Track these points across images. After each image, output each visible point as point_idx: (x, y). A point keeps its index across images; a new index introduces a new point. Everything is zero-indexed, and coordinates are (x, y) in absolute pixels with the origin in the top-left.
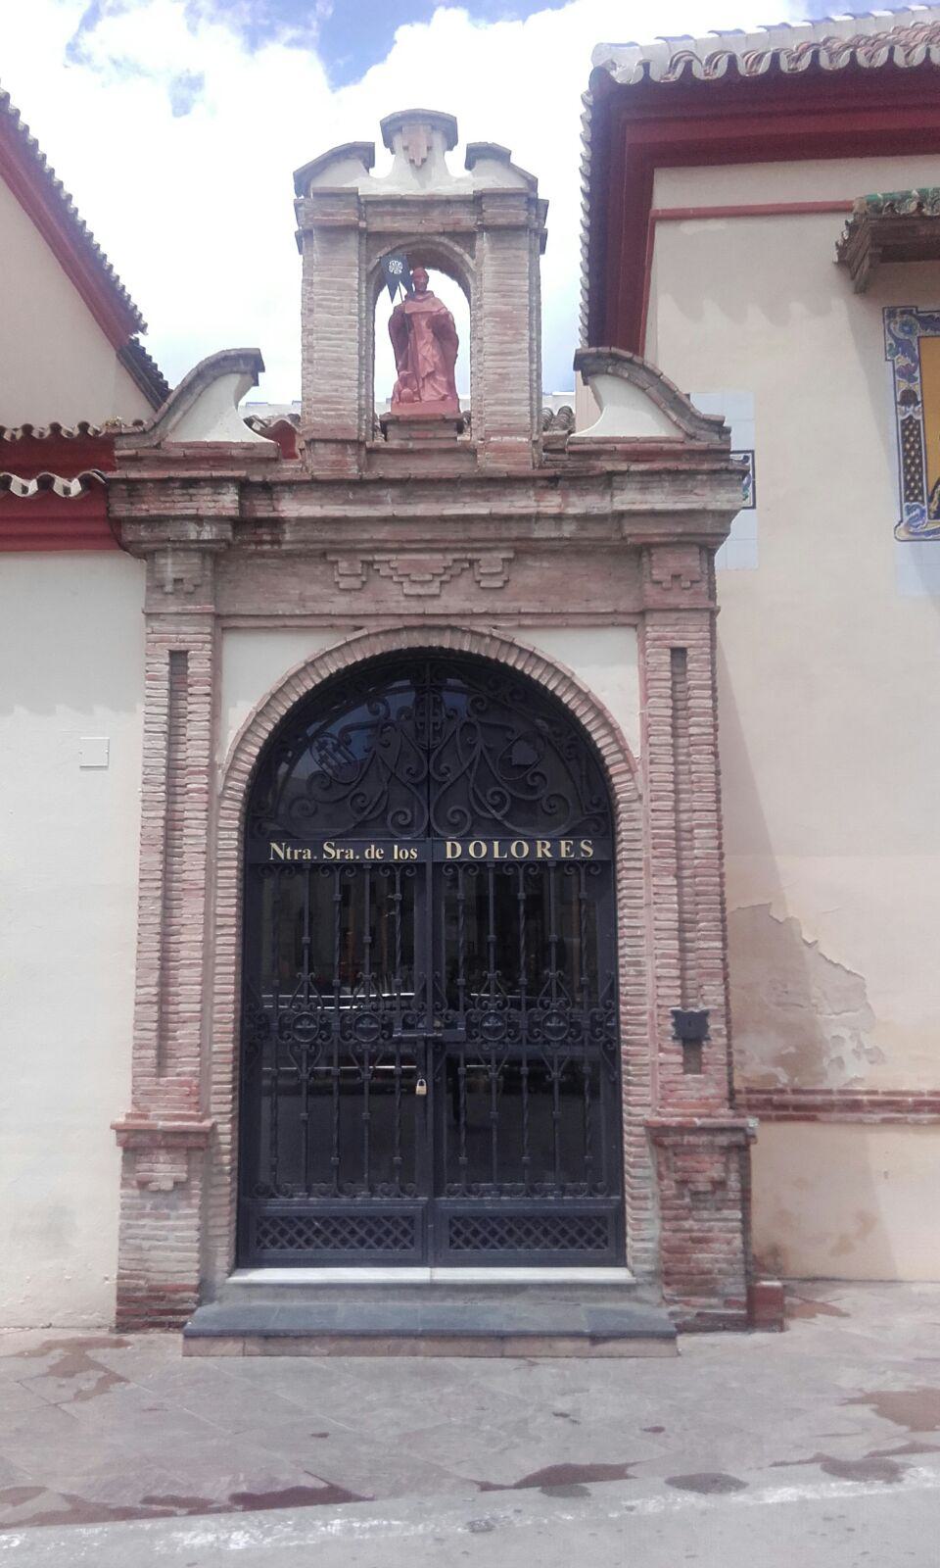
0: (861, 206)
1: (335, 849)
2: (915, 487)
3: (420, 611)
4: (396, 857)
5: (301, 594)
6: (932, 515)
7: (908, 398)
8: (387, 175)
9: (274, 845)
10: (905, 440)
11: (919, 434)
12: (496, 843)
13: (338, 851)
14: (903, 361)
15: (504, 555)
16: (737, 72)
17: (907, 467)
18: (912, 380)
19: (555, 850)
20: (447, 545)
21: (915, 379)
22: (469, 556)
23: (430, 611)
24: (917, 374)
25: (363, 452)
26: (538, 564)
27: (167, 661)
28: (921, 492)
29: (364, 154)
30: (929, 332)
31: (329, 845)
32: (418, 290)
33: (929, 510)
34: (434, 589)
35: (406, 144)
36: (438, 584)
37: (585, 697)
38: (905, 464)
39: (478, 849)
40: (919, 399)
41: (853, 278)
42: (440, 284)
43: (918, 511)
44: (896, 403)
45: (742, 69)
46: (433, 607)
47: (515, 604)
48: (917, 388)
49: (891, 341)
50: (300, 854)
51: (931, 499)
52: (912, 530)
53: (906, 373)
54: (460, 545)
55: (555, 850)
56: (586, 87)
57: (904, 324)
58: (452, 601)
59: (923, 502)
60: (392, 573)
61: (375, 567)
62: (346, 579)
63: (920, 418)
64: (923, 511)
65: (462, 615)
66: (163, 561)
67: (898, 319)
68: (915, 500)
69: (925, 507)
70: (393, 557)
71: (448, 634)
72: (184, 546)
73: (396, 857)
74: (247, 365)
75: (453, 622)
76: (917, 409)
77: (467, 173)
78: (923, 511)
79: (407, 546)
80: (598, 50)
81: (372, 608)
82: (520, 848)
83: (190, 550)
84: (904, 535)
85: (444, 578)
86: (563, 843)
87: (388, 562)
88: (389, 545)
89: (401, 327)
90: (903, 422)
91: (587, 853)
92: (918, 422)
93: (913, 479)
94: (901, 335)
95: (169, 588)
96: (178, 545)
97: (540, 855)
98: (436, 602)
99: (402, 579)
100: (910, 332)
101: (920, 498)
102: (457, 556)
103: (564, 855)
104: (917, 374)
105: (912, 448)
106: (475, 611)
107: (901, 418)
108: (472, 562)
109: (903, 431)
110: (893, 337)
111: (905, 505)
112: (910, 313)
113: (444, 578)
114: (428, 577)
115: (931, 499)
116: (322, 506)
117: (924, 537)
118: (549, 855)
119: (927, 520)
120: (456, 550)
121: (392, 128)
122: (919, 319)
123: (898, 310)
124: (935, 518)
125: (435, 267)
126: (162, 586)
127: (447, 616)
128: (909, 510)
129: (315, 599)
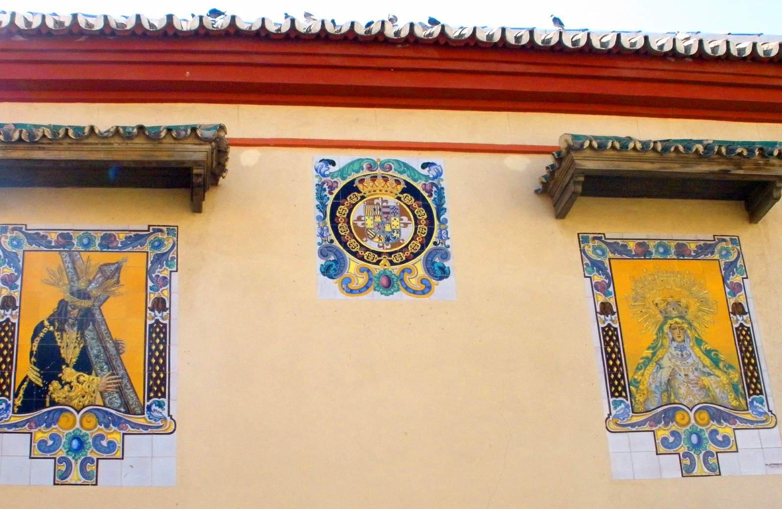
2: (156, 379)
6: (16, 410)
7: (606, 309)
10: (607, 344)
11: (617, 340)
14: (598, 278)
18: (607, 294)
21: (16, 287)
24: (18, 283)
30: (34, 247)
33: (14, 405)
38: (164, 359)
40: (18, 305)
44: (596, 313)
49: (586, 261)
51: (16, 395)
57: (595, 249)
59: (9, 397)
64: (8, 406)
67: (9, 235)
68: (620, 395)
69: (11, 402)
76: (14, 312)
78: (8, 406)
92: (14, 324)
93: (616, 378)
94: (594, 257)
101: (7, 393)
104: (18, 283)
107: (601, 325)
111: (611, 400)
112: (20, 230)
115: (16, 395)
117: (6, 429)
119: (11, 414)
122: (26, 235)
123: (10, 227)
124: (19, 412)
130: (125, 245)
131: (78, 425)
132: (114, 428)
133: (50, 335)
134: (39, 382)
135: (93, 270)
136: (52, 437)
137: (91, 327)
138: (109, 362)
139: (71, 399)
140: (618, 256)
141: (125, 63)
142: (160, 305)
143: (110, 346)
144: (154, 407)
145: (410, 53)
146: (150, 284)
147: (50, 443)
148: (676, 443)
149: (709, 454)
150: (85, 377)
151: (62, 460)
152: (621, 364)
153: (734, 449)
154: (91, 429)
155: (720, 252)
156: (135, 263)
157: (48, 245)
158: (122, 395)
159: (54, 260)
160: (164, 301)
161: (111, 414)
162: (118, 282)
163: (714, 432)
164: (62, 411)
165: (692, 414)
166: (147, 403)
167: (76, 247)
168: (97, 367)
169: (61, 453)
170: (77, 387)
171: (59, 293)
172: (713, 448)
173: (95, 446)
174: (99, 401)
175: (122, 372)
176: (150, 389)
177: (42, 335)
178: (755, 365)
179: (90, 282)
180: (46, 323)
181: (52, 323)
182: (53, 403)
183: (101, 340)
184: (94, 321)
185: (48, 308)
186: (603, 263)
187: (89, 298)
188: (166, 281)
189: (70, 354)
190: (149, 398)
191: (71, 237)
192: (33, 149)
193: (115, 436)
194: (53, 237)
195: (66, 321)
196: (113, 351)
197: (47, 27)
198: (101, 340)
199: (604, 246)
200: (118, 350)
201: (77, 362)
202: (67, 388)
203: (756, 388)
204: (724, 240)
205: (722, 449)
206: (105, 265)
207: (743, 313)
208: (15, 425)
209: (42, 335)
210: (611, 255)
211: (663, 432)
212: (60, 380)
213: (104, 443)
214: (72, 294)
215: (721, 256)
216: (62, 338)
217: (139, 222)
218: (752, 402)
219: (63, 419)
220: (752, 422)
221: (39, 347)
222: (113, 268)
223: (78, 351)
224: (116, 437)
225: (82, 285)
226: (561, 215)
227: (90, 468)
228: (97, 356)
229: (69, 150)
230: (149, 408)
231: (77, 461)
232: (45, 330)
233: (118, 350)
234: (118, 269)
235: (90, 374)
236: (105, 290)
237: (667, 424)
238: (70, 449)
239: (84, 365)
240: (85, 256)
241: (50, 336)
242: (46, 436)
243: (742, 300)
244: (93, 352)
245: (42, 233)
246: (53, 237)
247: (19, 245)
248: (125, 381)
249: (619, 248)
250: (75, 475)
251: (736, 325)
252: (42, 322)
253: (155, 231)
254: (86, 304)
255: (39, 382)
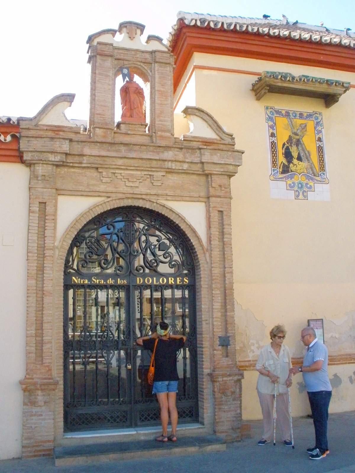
0: (265, 74)
1: (96, 280)
3: (132, 192)
4: (119, 283)
5: (88, 183)
7: (273, 135)
8: (119, 39)
9: (74, 278)
10: (272, 148)
12: (155, 278)
13: (98, 280)
14: (271, 123)
15: (163, 174)
16: (210, 26)
17: (273, 157)
18: (273, 129)
19: (175, 281)
20: (143, 169)
22: (150, 173)
23: (135, 192)
25: (113, 133)
26: (173, 178)
27: (38, 206)
28: (277, 165)
29: (113, 32)
30: (278, 115)
31: (94, 278)
32: (131, 79)
34: (137, 184)
35: (128, 32)
36: (138, 183)
37: (190, 226)
39: (148, 281)
41: (256, 95)
42: (137, 79)
43: (276, 171)
45: (225, 26)
46: (136, 191)
47: (165, 192)
48: (275, 132)
50: (83, 281)
51: (280, 168)
52: (275, 177)
53: (271, 127)
54: (147, 169)
55: (175, 281)
56: (175, 23)
57: (271, 112)
58: (143, 189)
60: (122, 177)
61: (116, 175)
62: (105, 179)
63: (276, 142)
65: (147, 195)
66: (38, 168)
70: (122, 172)
71: (141, 201)
72: (47, 162)
73: (119, 283)
74: (69, 98)
75: (144, 197)
77: (146, 44)
79: (128, 168)
80: (180, 13)
81: (114, 190)
82: (163, 281)
83: (48, 164)
84: (272, 178)
85: (140, 181)
86: (178, 279)
87: (121, 173)
88: (122, 167)
89: (125, 91)
90: (271, 142)
91: (186, 282)
94: (270, 115)
95: (39, 178)
96: (44, 162)
97: (170, 283)
98: (137, 189)
99: (125, 180)
100: (273, 114)
102: (146, 173)
103: (178, 283)
105: (274, 151)
106: (151, 193)
107: (271, 141)
108: (150, 175)
109: (271, 145)
110: (268, 115)
111: (272, 169)
113: (140, 181)
114: (135, 180)
115: (280, 168)
116: (99, 151)
118: (173, 283)
120: (146, 170)
121: (123, 26)
122: (275, 111)
125: (137, 74)
126: (37, 177)
127: (141, 194)
128: (274, 170)
129: (93, 185)
130: (307, 117)
131: (300, 179)
132: (311, 181)
133: (287, 147)
134: (286, 164)
135: (298, 125)
136: (293, 183)
137: (300, 146)
138: (307, 158)
139: (297, 170)
140: (279, 116)
141: (196, 37)
142: (320, 140)
143: (307, 152)
144: (322, 175)
145: (233, 35)
146: (316, 132)
147: (292, 185)
148: (293, 187)
149: (304, 191)
150: (300, 163)
151: (297, 191)
152: (277, 156)
153: (313, 190)
154: (304, 181)
155: (315, 118)
156: (310, 124)
157: (282, 115)
158: (312, 170)
159: (285, 120)
160: (274, 134)
161: (309, 176)
162: (306, 131)
163: (307, 184)
164: (295, 174)
165: (300, 176)
166: (320, 173)
167: (292, 117)
168: (303, 160)
169: (296, 188)
170: (298, 166)
171: (289, 133)
172: (306, 190)
173: (306, 187)
174: (306, 171)
175: (311, 162)
176: (320, 169)
177: (285, 147)
178: (323, 160)
179: (298, 130)
180: (286, 143)
181: (288, 143)
182: (292, 171)
183: (303, 150)
184: (301, 144)
185: (285, 139)
186: (273, 118)
187: (298, 135)
188: (320, 132)
189: (295, 154)
190: (320, 171)
191: (289, 113)
192: (285, 83)
193: (311, 183)
194: (284, 112)
195: (292, 143)
196: (308, 154)
197: (197, 25)
198: (303, 150)
199: (274, 111)
200: (309, 154)
201: (298, 157)
202: (295, 166)
203: (323, 169)
204: (317, 113)
205: (309, 190)
206: (301, 124)
207: (321, 141)
208: (281, 178)
209: (285, 147)
210: (276, 115)
211: (289, 182)
212: (293, 163)
213: (308, 186)
214: (293, 133)
215: (315, 119)
216: (291, 149)
217: (310, 111)
218: (321, 174)
219: (295, 177)
220: (320, 181)
221: (285, 151)
222: (304, 125)
223: (297, 154)
224: (312, 184)
225: (295, 131)
226: (258, 99)
227: (305, 194)
228: (303, 156)
229: (302, 85)
230: (321, 174)
231: (301, 191)
232: (286, 145)
233: (309, 154)
234: (306, 126)
235: (302, 162)
236: (303, 133)
237: (291, 179)
238: (299, 188)
239: (299, 159)
240: (295, 120)
241: (287, 148)
242: (291, 182)
243: (321, 136)
244: (302, 154)
245: (280, 110)
246: (284, 112)
247: (273, 114)
248: (313, 165)
249: (278, 112)
250: (301, 196)
251: (318, 145)
252: (285, 143)
253: (316, 113)
254: (298, 137)
255: (286, 164)
